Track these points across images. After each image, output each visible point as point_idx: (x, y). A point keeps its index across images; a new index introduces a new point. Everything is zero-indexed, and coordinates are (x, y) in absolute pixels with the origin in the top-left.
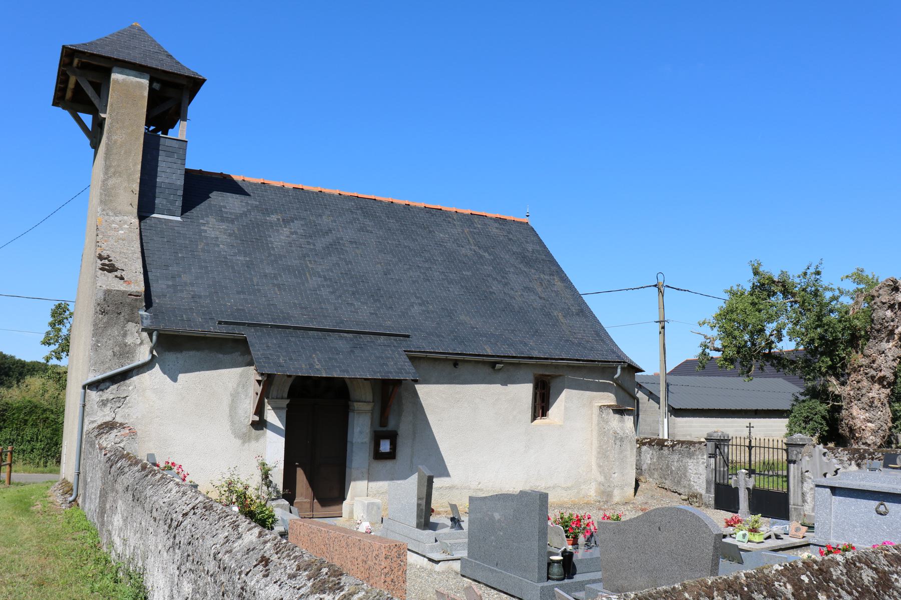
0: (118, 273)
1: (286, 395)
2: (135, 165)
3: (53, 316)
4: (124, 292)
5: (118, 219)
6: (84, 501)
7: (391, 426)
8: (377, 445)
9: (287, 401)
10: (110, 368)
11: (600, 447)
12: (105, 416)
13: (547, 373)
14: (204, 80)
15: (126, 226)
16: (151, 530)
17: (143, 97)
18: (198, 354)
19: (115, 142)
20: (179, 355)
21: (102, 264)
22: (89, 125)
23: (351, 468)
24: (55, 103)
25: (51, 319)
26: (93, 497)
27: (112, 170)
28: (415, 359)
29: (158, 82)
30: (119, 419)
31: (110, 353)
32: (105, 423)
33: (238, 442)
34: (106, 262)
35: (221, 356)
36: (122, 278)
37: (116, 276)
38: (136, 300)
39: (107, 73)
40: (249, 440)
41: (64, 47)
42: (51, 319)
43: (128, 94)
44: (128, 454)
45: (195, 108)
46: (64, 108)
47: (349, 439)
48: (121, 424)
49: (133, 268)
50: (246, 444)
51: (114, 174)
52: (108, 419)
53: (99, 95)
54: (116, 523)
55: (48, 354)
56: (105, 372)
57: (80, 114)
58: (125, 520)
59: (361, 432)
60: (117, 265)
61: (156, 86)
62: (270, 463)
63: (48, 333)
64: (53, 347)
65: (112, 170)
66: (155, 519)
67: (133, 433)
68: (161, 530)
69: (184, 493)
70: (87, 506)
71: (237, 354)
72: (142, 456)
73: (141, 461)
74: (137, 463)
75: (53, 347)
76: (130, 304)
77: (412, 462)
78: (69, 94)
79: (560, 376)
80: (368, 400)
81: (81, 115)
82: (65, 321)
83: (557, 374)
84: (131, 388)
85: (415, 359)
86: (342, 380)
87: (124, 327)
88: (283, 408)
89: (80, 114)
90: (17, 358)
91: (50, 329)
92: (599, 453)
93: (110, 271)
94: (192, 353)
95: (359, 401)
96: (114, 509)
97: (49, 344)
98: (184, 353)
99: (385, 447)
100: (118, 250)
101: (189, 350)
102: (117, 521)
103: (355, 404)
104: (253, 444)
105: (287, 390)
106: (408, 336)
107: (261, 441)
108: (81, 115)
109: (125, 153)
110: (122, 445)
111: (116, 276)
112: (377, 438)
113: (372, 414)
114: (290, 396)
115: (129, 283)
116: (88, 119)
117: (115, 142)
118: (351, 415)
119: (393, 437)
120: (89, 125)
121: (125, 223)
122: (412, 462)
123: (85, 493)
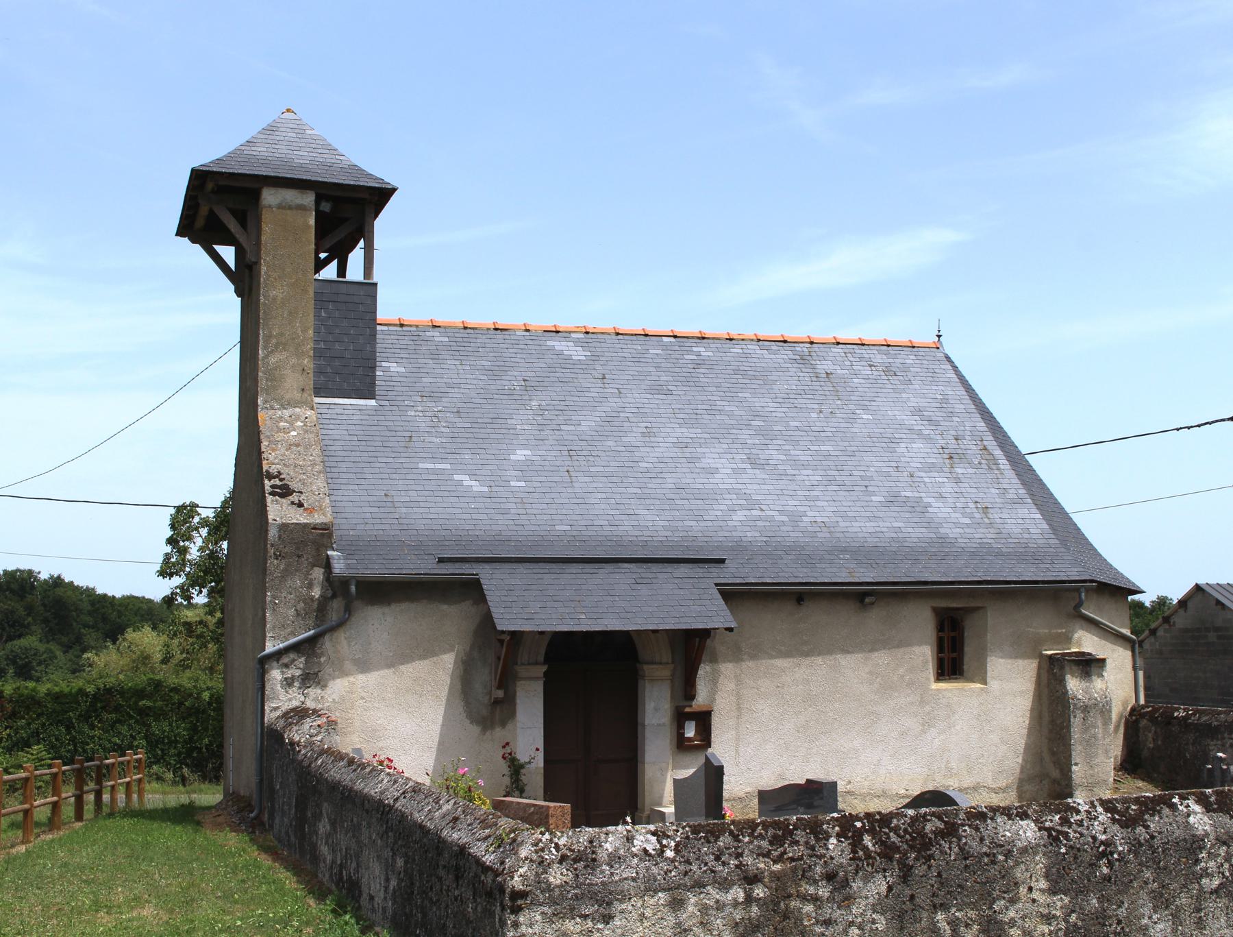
0: (295, 498)
1: (541, 658)
2: (305, 331)
3: (173, 527)
4: (306, 525)
5: (287, 413)
6: (272, 817)
7: (701, 699)
8: (680, 727)
9: (545, 668)
10: (293, 634)
11: (1052, 722)
12: (290, 700)
13: (954, 605)
14: (394, 190)
15: (299, 424)
16: (364, 823)
17: (309, 227)
18: (413, 606)
19: (275, 299)
20: (386, 610)
21: (272, 486)
22: (231, 263)
23: (643, 763)
24: (180, 233)
25: (169, 533)
26: (286, 807)
27: (274, 341)
28: (732, 595)
29: (327, 201)
30: (310, 704)
31: (292, 612)
32: (292, 710)
33: (475, 730)
34: (277, 482)
35: (445, 607)
36: (300, 505)
37: (293, 503)
38: (322, 535)
39: (255, 196)
40: (492, 727)
41: (193, 170)
42: (169, 533)
43: (287, 225)
44: (329, 748)
45: (384, 225)
46: (194, 241)
47: (639, 720)
48: (315, 711)
49: (314, 488)
50: (488, 733)
51: (277, 346)
52: (295, 703)
53: (243, 223)
54: (321, 831)
55: (168, 592)
56: (287, 639)
57: (216, 247)
58: (333, 824)
59: (656, 710)
60: (294, 485)
61: (326, 207)
62: (522, 757)
63: (167, 557)
64: (178, 581)
65: (274, 341)
66: (367, 811)
67: (332, 724)
68: (374, 820)
69: (395, 782)
70: (277, 821)
71: (468, 603)
72: (346, 749)
73: (347, 754)
74: (342, 759)
75: (178, 581)
76: (314, 542)
77: (737, 752)
78: (200, 222)
79: (978, 608)
80: (664, 660)
81: (220, 249)
82: (194, 533)
83: (973, 605)
84: (322, 660)
85: (732, 595)
86: (626, 634)
87: (308, 574)
88: (537, 678)
89: (216, 247)
90: (100, 591)
91: (169, 549)
92: (1051, 731)
93: (282, 496)
94: (404, 606)
95: (653, 663)
96: (318, 817)
97: (171, 575)
98: (393, 606)
99: (690, 732)
100: (291, 462)
101: (399, 601)
102: (324, 827)
103: (645, 667)
104: (499, 732)
105: (543, 651)
106: (722, 561)
107: (510, 726)
108: (220, 249)
109: (290, 313)
110: (319, 738)
111: (293, 503)
112: (681, 717)
113: (672, 681)
114: (547, 660)
115: (311, 511)
116: (228, 253)
117: (275, 299)
118: (640, 683)
119: (704, 720)
120: (231, 263)
121: (298, 419)
122: (737, 752)
123: (273, 806)
